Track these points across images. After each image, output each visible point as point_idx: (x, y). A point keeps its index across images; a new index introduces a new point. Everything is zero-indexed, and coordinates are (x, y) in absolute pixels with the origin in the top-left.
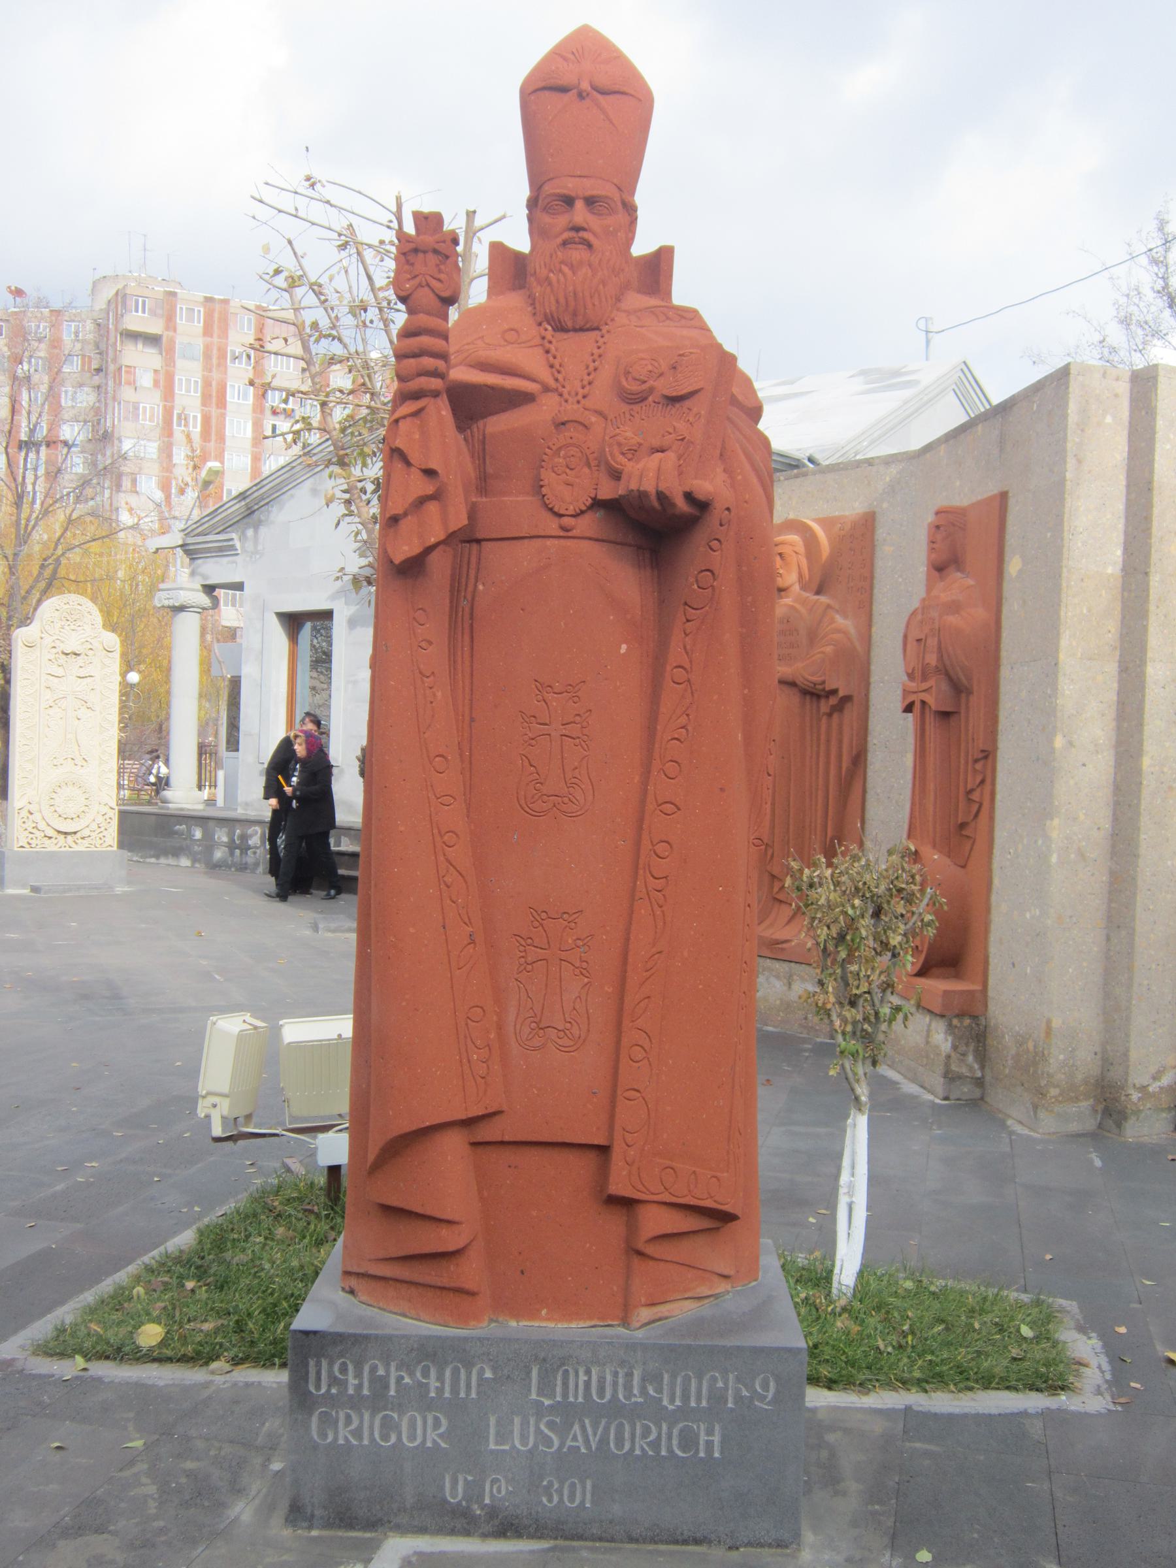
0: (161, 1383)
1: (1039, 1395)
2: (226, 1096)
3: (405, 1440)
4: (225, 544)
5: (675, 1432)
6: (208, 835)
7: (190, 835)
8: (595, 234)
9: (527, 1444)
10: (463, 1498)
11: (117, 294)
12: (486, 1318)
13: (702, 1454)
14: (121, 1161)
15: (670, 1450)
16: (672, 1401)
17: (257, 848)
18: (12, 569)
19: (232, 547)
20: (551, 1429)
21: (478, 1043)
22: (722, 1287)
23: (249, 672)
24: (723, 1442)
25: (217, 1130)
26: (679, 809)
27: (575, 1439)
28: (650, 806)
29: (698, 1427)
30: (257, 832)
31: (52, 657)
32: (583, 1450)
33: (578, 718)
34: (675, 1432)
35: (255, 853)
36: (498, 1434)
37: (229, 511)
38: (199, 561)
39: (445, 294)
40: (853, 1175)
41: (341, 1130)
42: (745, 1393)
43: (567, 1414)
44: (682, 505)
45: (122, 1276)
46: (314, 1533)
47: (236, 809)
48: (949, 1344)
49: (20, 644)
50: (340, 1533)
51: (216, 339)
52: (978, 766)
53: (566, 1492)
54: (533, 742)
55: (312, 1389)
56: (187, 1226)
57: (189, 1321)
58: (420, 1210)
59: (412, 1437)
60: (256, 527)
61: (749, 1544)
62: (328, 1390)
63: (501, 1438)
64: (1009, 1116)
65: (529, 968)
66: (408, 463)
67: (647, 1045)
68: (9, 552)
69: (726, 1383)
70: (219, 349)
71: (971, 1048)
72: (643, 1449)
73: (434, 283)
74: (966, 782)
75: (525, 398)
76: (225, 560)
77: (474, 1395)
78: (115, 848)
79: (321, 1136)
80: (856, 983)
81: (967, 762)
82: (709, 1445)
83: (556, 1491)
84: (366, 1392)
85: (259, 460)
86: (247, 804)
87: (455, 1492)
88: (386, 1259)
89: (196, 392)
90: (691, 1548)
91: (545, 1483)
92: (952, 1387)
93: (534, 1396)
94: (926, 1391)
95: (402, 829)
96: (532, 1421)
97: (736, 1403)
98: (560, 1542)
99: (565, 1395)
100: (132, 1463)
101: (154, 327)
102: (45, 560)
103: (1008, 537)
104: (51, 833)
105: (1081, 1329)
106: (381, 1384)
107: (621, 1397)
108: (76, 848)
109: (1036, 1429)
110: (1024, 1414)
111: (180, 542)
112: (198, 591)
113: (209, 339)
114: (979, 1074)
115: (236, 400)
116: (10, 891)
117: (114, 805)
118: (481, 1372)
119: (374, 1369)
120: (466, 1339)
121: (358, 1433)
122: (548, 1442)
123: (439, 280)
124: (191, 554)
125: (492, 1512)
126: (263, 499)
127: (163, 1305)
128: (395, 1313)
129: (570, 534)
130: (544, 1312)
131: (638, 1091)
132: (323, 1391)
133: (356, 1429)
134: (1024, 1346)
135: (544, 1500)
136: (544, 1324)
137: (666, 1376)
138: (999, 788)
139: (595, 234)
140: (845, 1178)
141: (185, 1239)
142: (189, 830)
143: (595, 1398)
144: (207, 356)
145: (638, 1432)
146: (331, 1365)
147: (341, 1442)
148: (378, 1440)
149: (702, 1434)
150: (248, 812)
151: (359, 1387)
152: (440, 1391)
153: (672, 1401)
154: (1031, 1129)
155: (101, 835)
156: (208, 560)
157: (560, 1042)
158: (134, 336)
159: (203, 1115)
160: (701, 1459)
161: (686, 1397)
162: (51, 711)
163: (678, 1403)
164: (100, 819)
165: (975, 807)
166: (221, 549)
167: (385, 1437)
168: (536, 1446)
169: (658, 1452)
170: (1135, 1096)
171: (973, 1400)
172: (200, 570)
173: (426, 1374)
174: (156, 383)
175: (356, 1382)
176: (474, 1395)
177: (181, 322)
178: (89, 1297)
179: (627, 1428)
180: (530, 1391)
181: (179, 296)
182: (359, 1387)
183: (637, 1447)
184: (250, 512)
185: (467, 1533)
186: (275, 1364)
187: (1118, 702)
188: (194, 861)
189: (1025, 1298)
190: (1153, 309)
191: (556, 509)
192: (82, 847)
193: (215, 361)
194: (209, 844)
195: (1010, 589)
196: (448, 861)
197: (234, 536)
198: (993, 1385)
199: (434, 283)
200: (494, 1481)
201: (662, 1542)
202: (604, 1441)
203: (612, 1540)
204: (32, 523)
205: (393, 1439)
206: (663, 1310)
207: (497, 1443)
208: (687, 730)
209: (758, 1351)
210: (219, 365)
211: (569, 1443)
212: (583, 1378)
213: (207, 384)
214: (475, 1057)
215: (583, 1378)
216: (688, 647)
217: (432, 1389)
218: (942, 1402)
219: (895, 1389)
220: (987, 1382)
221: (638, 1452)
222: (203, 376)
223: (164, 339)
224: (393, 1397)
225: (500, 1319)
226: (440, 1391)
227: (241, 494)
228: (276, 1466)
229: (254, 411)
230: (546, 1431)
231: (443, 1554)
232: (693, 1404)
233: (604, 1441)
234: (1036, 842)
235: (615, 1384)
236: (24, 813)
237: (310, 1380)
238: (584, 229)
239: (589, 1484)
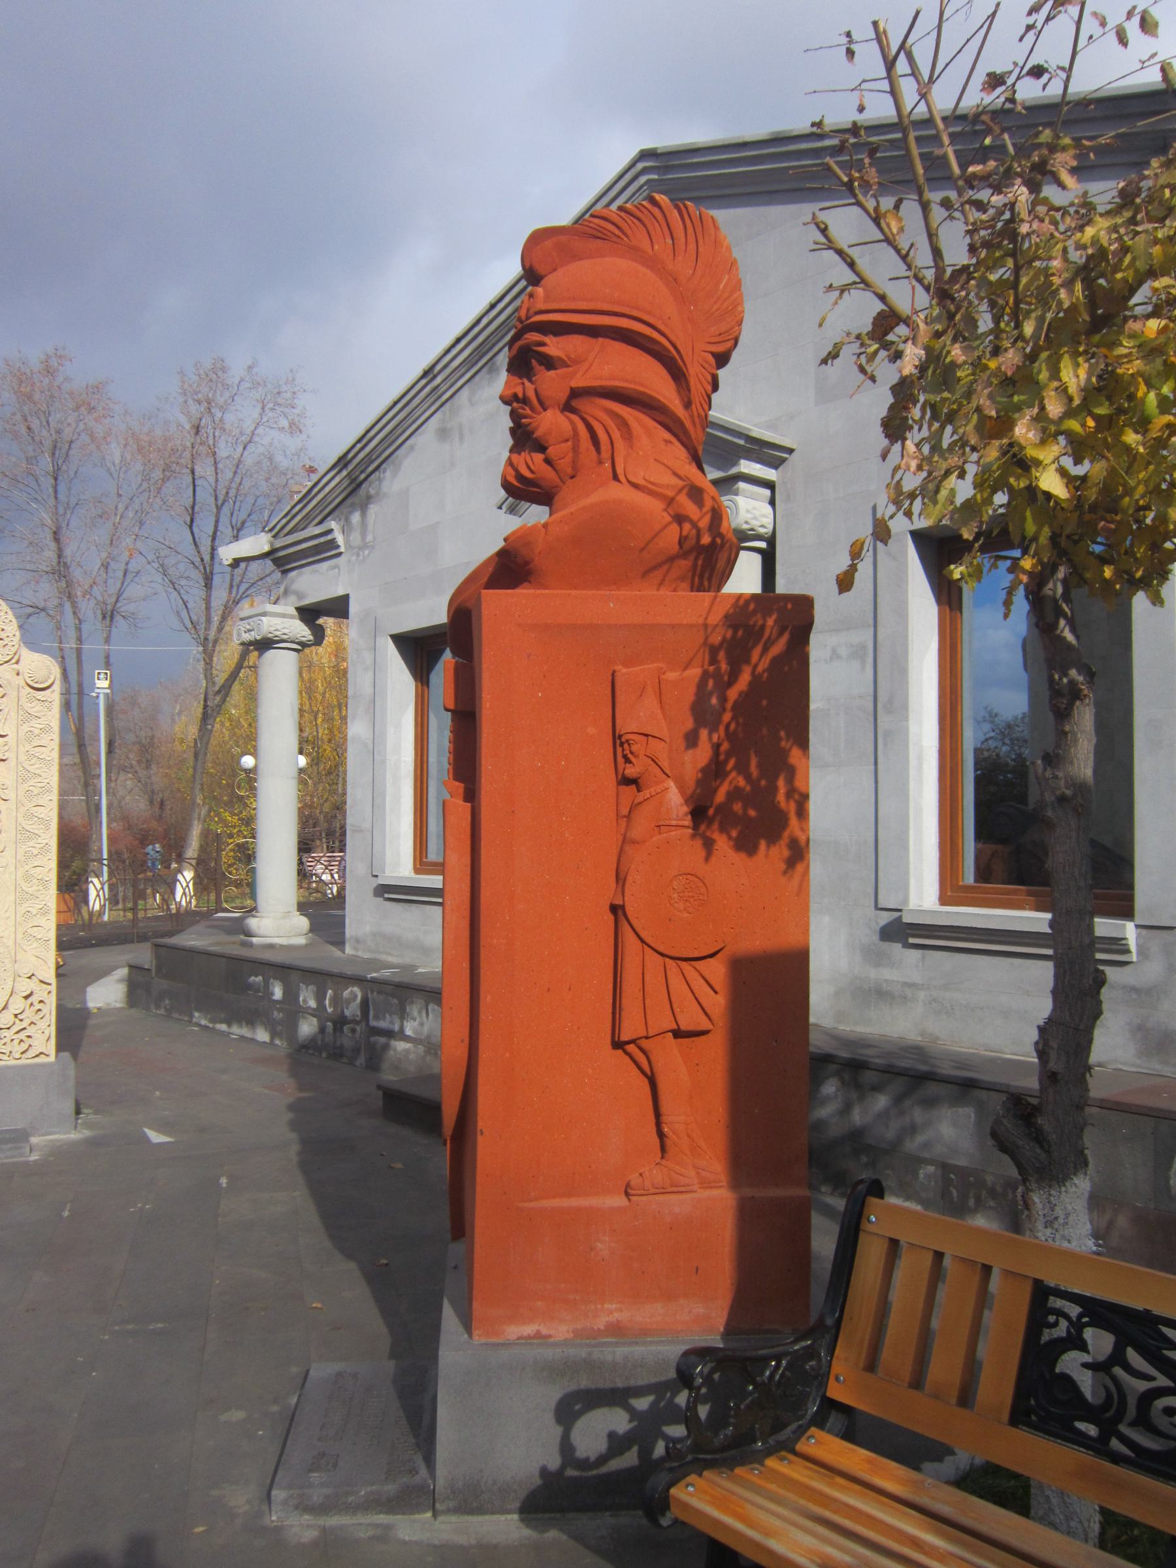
4: (322, 540)
6: (291, 995)
19: (332, 544)
30: (356, 996)
35: (353, 1031)
37: (327, 489)
38: (293, 574)
60: (364, 508)
76: (325, 565)
86: (358, 941)
111: (267, 548)
112: (292, 617)
124: (283, 565)
126: (372, 462)
150: (360, 954)
155: (22, 1035)
156: (304, 569)
166: (318, 550)
188: (274, 1035)
197: (333, 525)
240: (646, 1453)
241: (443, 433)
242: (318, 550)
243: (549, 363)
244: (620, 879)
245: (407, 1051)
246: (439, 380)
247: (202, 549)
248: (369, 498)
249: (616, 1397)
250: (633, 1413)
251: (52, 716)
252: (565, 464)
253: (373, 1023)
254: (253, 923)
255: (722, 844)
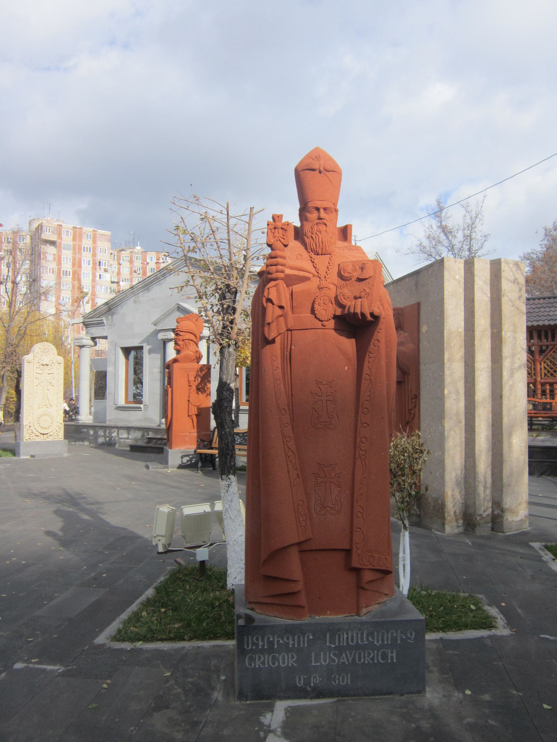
0: (165, 649)
1: (485, 630)
2: (164, 536)
3: (281, 664)
5: (380, 654)
6: (96, 433)
7: (88, 433)
8: (327, 221)
9: (326, 662)
10: (304, 684)
11: (39, 225)
12: (308, 616)
13: (389, 661)
14: (112, 563)
15: (378, 661)
16: (378, 642)
17: (116, 437)
18: (7, 331)
19: (103, 323)
20: (335, 656)
21: (302, 514)
22: (385, 599)
23: (110, 370)
24: (397, 655)
25: (161, 550)
26: (369, 425)
27: (343, 659)
28: (359, 425)
29: (388, 651)
31: (38, 367)
32: (347, 663)
33: (332, 394)
34: (380, 654)
36: (315, 659)
37: (102, 309)
38: (89, 328)
39: (285, 244)
40: (404, 554)
41: (204, 547)
42: (404, 637)
43: (340, 650)
44: (369, 318)
45: (134, 607)
46: (248, 702)
47: (106, 422)
48: (447, 614)
49: (25, 361)
50: (258, 702)
51: (77, 243)
52: (413, 401)
53: (341, 679)
54: (316, 403)
55: (246, 648)
56: (149, 587)
57: (168, 624)
58: (283, 577)
59: (284, 663)
60: (112, 315)
61: (408, 693)
62: (252, 648)
63: (316, 661)
64: (432, 528)
65: (318, 485)
66: (273, 304)
67: (361, 511)
68: (6, 325)
69: (397, 634)
70: (79, 246)
71: (416, 504)
72: (368, 661)
73: (282, 240)
74: (409, 406)
75: (308, 279)
77: (306, 645)
78: (63, 439)
79: (198, 550)
80: (403, 483)
81: (408, 400)
82: (392, 657)
83: (337, 679)
84: (266, 647)
85: (95, 287)
86: (110, 420)
87: (300, 682)
88: (268, 596)
89: (70, 262)
90: (387, 696)
91: (333, 676)
92: (454, 630)
93: (328, 644)
94: (445, 632)
95: (273, 436)
96: (328, 653)
97: (401, 641)
98: (340, 698)
99: (339, 643)
100: (168, 681)
101: (54, 238)
102: (20, 328)
103: (421, 318)
104: (38, 434)
105: (489, 605)
106: (271, 644)
107: (360, 642)
108: (48, 440)
109: (488, 642)
110: (482, 638)
111: (82, 321)
112: (89, 339)
113: (75, 242)
114: (419, 513)
115: (85, 265)
116: (22, 457)
117: (62, 422)
118: (308, 636)
119: (269, 638)
120: (301, 625)
121: (263, 663)
122: (334, 661)
123: (283, 239)
125: (314, 689)
127: (156, 618)
128: (273, 616)
129: (326, 328)
130: (328, 612)
131: (360, 528)
132: (250, 648)
133: (263, 661)
134: (474, 613)
135: (333, 683)
136: (328, 617)
137: (375, 633)
138: (421, 408)
139: (327, 221)
140: (401, 555)
141: (150, 592)
142: (88, 431)
143: (350, 643)
144: (74, 249)
145: (366, 654)
146: (252, 637)
147: (257, 666)
148: (271, 665)
149: (389, 653)
150: (111, 423)
151: (263, 646)
152: (293, 645)
153: (378, 642)
154: (441, 532)
157: (331, 512)
158: (47, 242)
159: (155, 544)
160: (389, 663)
161: (383, 641)
162: (37, 387)
163: (380, 643)
164: (57, 428)
165: (412, 416)
166: (98, 324)
167: (274, 664)
168: (329, 663)
169: (374, 662)
170: (478, 518)
171: (463, 634)
172: (90, 332)
173: (288, 639)
174: (54, 259)
175: (262, 644)
176: (306, 645)
177: (64, 236)
178: (124, 616)
179: (362, 653)
180: (326, 642)
181: (63, 226)
182: (263, 646)
183: (366, 660)
184: (110, 309)
185: (305, 698)
186: (207, 639)
187: (465, 377)
188: (90, 443)
189: (466, 595)
190: (437, 233)
191: (321, 319)
192: (50, 439)
193: (77, 251)
194: (96, 436)
195: (422, 337)
196: (288, 447)
197: (104, 318)
198: (469, 628)
199: (282, 240)
200: (314, 677)
201: (377, 695)
202: (354, 659)
203: (358, 696)
204: (15, 314)
205: (277, 664)
206: (370, 608)
207: (315, 662)
208: (370, 397)
209: (408, 622)
210: (79, 252)
211: (341, 661)
212: (345, 636)
213: (74, 259)
214: (301, 519)
215: (345, 636)
216: (370, 367)
217: (290, 644)
218: (452, 635)
219: (434, 632)
220: (466, 627)
221: (366, 662)
222: (73, 256)
223: (58, 242)
224: (276, 648)
225: (312, 616)
226: (293, 645)
227: (106, 303)
228: (223, 678)
229: (92, 269)
230: (333, 657)
231: (298, 706)
232: (386, 643)
233: (354, 659)
234: (438, 428)
235: (357, 637)
236: (28, 427)
237: (224, 644)
238: (323, 219)
239: (349, 675)
240: (191, 462)
241: (135, 302)
242: (98, 324)
243: (180, 335)
244: (189, 397)
245: (130, 442)
246: (134, 290)
247: (9, 294)
248: (114, 313)
249: (188, 456)
250: (190, 458)
251: (62, 370)
252: (182, 347)
253: (120, 436)
254: (79, 417)
255: (200, 393)
